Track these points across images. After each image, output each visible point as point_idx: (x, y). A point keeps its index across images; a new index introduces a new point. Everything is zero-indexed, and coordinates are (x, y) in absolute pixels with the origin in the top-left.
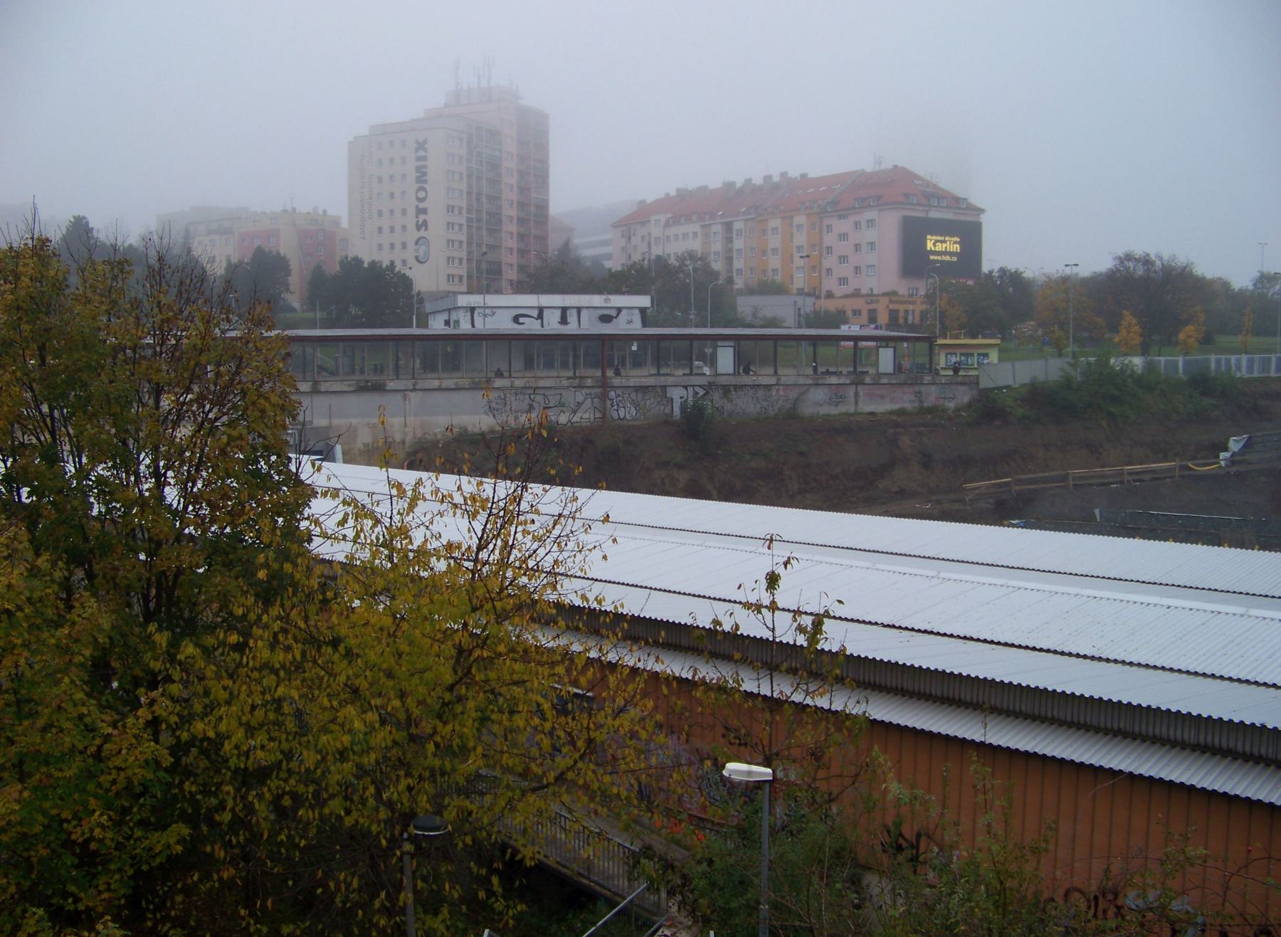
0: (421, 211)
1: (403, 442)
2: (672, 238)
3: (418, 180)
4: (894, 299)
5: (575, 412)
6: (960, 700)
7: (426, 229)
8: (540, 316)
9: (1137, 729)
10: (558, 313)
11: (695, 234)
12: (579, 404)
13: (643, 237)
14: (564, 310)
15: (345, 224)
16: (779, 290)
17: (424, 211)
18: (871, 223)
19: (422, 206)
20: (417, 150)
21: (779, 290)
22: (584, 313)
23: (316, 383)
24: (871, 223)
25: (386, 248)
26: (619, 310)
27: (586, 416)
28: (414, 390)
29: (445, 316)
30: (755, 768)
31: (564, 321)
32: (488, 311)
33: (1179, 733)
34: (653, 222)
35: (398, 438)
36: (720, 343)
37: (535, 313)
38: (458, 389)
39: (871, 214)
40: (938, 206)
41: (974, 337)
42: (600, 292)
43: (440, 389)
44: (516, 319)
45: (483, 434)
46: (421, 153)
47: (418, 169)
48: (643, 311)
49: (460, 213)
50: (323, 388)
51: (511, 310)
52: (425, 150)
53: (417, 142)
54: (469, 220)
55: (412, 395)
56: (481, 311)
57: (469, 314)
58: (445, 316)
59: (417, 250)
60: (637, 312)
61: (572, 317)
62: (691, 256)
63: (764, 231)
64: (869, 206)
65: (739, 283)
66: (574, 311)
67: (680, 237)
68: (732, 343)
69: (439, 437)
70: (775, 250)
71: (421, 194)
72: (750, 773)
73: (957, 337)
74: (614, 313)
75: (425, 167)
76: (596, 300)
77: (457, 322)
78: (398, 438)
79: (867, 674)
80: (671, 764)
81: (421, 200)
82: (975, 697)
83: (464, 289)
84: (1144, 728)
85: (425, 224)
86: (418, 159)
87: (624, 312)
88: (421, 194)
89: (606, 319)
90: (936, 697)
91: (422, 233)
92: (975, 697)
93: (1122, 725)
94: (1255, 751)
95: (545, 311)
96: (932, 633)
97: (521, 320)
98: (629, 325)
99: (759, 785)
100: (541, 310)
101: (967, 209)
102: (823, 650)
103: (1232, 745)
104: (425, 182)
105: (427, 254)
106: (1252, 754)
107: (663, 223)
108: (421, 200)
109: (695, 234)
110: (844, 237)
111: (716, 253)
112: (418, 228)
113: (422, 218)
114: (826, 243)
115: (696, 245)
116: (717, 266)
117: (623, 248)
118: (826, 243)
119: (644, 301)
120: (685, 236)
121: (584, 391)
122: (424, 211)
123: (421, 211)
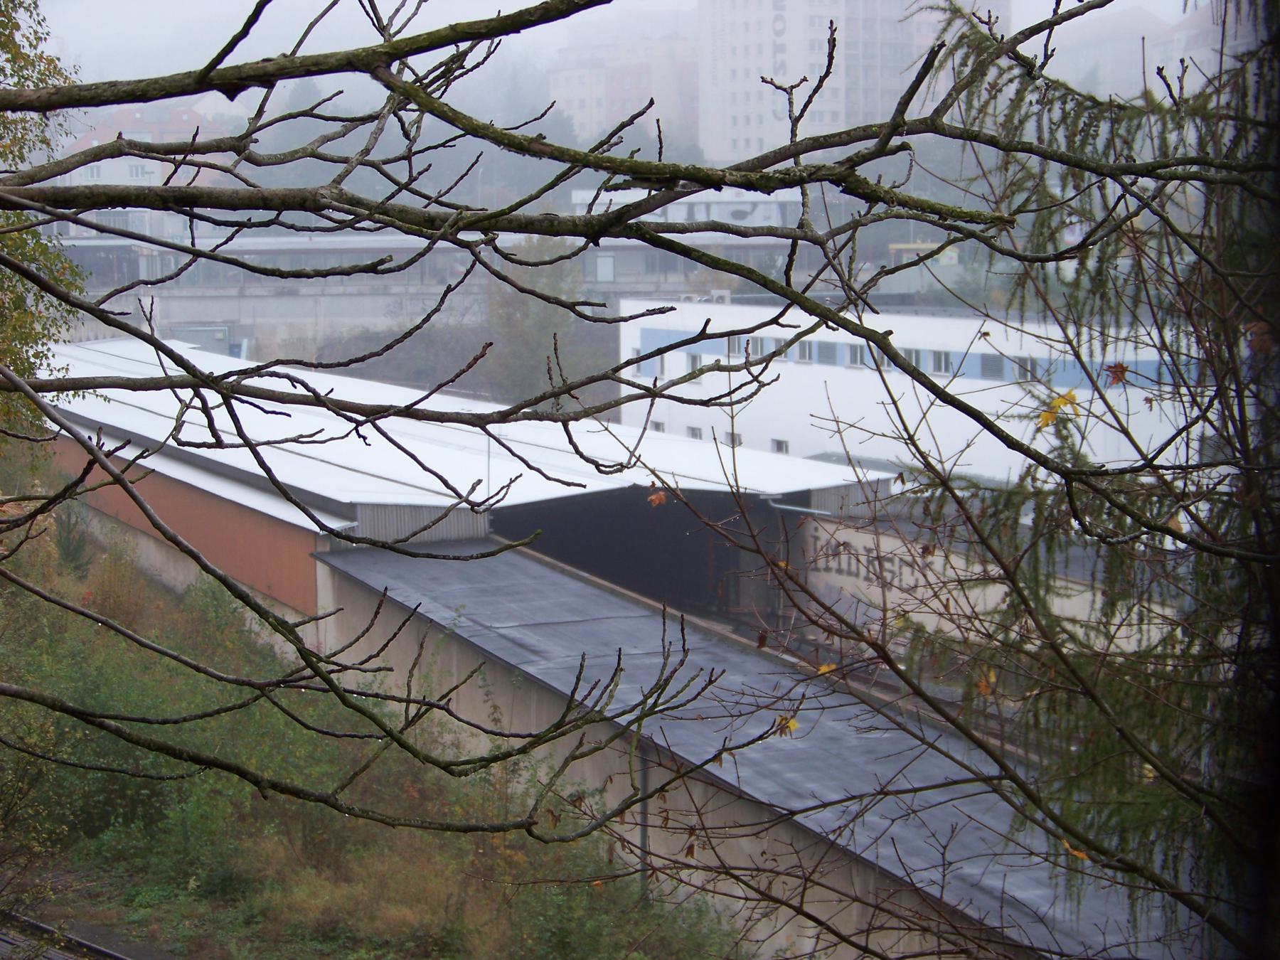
0: (779, 49)
1: (315, 339)
5: (463, 315)
7: (784, 74)
12: (467, 309)
23: (242, 289)
27: (473, 319)
28: (323, 295)
35: (310, 335)
38: (360, 294)
43: (344, 295)
45: (377, 334)
50: (248, 292)
55: (322, 299)
66: (703, 208)
69: (345, 334)
74: (747, 208)
78: (310, 335)
80: (1169, 628)
81: (779, 33)
88: (779, 26)
108: (779, 33)
113: (780, 57)
121: (472, 297)
123: (779, 49)
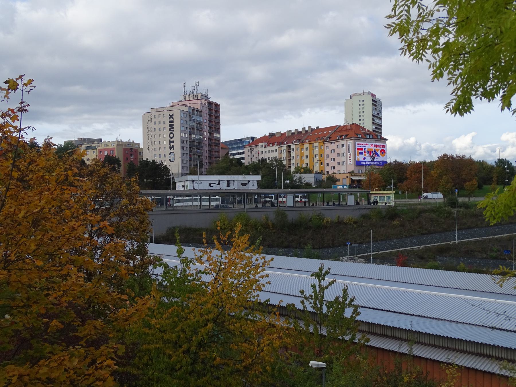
2: (267, 152)
3: (170, 130)
4: (353, 174)
6: (387, 335)
7: (173, 149)
8: (219, 184)
9: (454, 347)
10: (226, 182)
11: (276, 150)
13: (256, 151)
14: (228, 181)
15: (141, 146)
16: (308, 171)
17: (173, 142)
18: (343, 145)
19: (172, 140)
20: (170, 118)
21: (308, 171)
22: (236, 182)
24: (343, 145)
25: (158, 156)
26: (249, 181)
29: (182, 183)
30: (320, 363)
31: (228, 185)
32: (200, 182)
33: (471, 349)
34: (260, 146)
36: (288, 195)
37: (217, 183)
39: (343, 142)
40: (370, 138)
41: (384, 190)
42: (241, 174)
44: (210, 185)
46: (171, 119)
47: (170, 126)
48: (258, 181)
49: (187, 143)
51: (208, 181)
52: (173, 118)
53: (170, 115)
54: (190, 145)
56: (198, 182)
57: (192, 183)
58: (182, 183)
59: (170, 157)
60: (256, 182)
61: (231, 184)
62: (276, 160)
63: (303, 149)
64: (343, 139)
65: (292, 169)
67: (271, 151)
68: (293, 195)
70: (307, 156)
71: (171, 135)
72: (318, 365)
73: (378, 190)
74: (247, 182)
75: (173, 125)
76: (240, 177)
77: (187, 186)
79: (386, 332)
82: (381, 332)
83: (188, 172)
84: (471, 349)
85: (173, 146)
86: (170, 122)
87: (251, 182)
88: (171, 135)
89: (244, 184)
90: (378, 334)
91: (172, 150)
92: (381, 332)
93: (449, 346)
94: (500, 356)
95: (221, 181)
96: (405, 314)
97: (212, 185)
98: (253, 187)
99: (321, 369)
100: (219, 181)
101: (381, 139)
102: (357, 320)
103: (491, 353)
104: (173, 131)
105: (174, 158)
106: (499, 357)
107: (264, 146)
109: (276, 150)
110: (333, 151)
111: (284, 158)
112: (170, 148)
113: (172, 144)
114: (326, 154)
115: (276, 155)
116: (285, 162)
117: (249, 156)
118: (326, 154)
119: (258, 178)
120: (273, 151)
122: (173, 142)
